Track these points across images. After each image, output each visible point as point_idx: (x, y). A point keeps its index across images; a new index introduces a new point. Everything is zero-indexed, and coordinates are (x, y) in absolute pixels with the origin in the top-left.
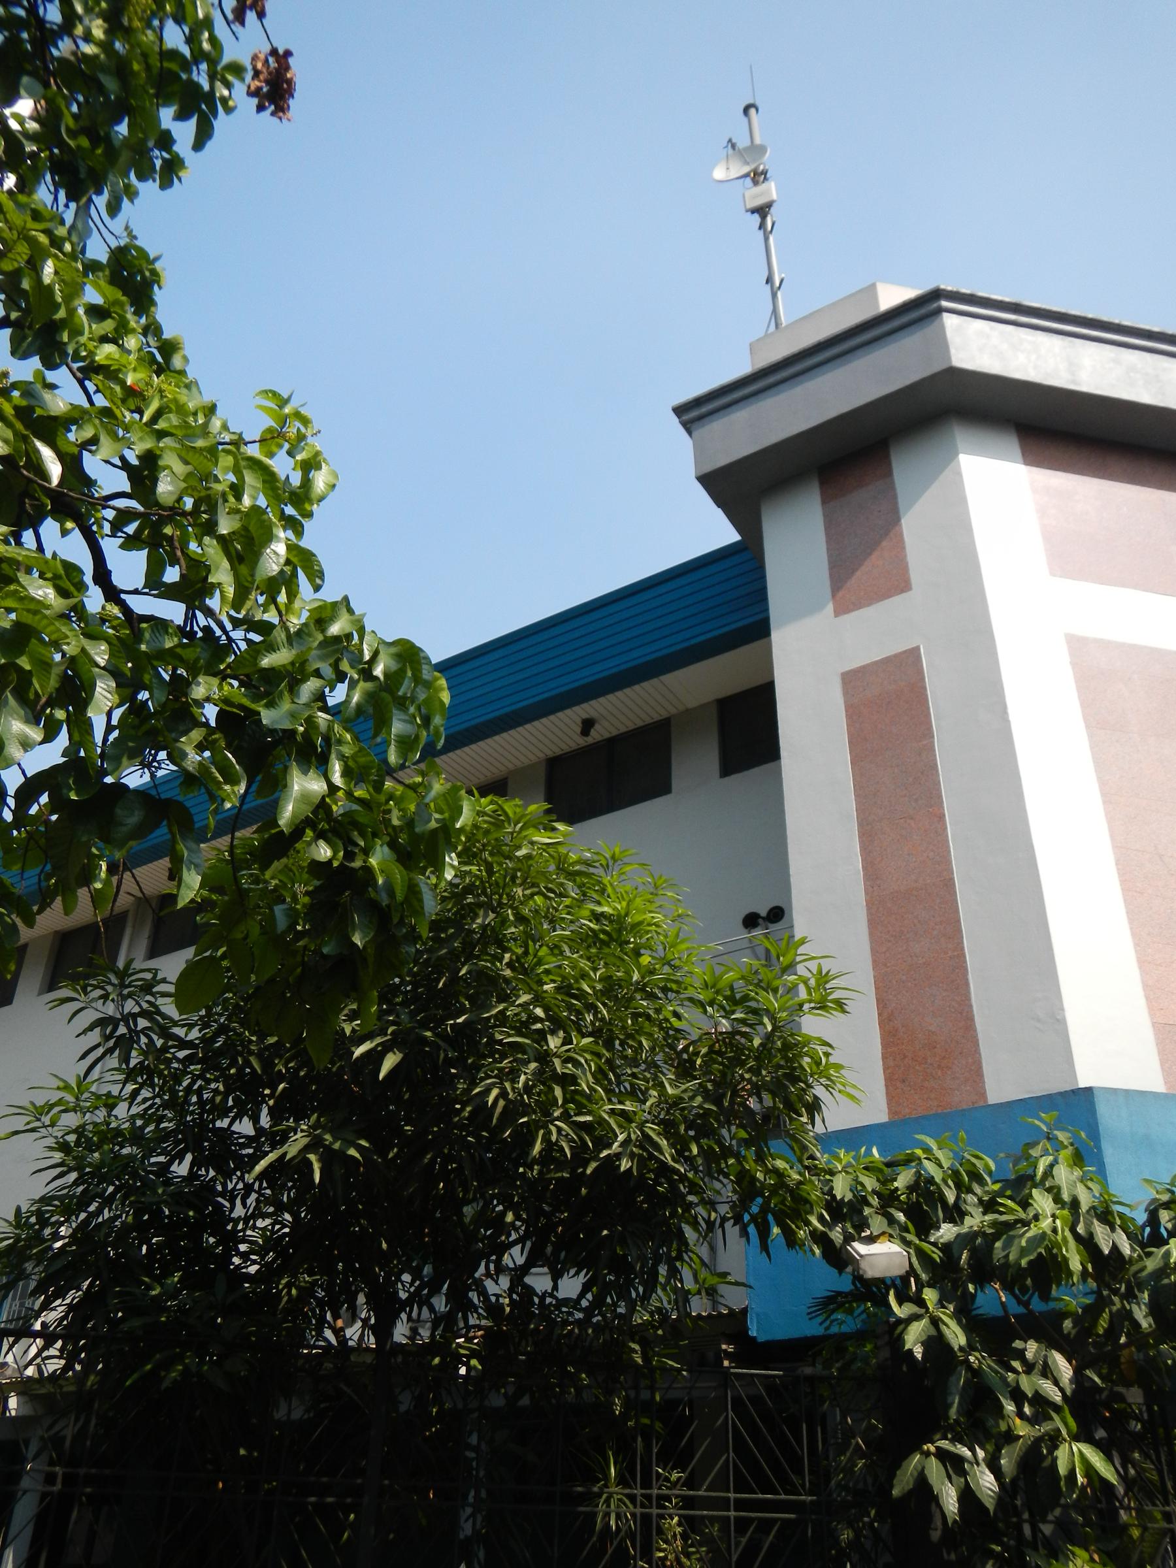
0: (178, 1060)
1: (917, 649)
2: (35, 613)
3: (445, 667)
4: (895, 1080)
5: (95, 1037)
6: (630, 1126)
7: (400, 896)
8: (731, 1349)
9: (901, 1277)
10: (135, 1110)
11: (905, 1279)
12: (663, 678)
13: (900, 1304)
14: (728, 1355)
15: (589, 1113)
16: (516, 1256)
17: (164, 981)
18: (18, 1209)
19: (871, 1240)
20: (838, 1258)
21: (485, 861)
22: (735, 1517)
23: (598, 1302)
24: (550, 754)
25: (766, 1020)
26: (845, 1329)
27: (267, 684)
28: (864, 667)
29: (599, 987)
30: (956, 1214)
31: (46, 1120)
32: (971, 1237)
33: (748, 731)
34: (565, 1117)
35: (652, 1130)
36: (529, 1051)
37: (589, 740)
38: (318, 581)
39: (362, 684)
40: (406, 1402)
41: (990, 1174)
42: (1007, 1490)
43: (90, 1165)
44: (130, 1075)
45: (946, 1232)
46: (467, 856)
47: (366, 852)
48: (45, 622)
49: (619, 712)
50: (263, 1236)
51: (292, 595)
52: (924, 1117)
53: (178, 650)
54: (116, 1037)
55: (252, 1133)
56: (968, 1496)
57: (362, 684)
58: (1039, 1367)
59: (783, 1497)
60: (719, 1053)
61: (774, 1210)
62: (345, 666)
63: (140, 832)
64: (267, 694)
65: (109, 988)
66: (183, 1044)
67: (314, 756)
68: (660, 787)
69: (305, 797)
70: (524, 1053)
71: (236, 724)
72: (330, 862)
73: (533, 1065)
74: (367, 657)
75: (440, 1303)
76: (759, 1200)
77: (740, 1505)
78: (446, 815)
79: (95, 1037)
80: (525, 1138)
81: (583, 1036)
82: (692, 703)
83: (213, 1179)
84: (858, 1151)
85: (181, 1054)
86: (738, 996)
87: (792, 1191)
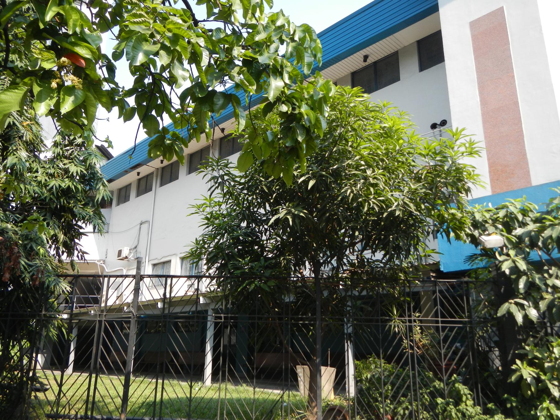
0: (239, 189)
1: (503, 7)
2: (179, 28)
3: (320, 35)
4: (493, 180)
5: (212, 183)
6: (398, 199)
7: (313, 122)
8: (434, 275)
9: (500, 247)
10: (228, 206)
11: (502, 248)
12: (394, 35)
13: (500, 255)
14: (433, 277)
15: (383, 196)
16: (358, 246)
17: (231, 163)
18: (196, 239)
19: (489, 235)
20: (475, 241)
21: (339, 109)
22: (442, 326)
23: (389, 260)
24: (352, 71)
25: (449, 160)
26: (478, 266)
27: (259, 47)
28: (479, 18)
29: (384, 152)
30: (523, 224)
31: (201, 210)
32: (529, 233)
33: (431, 52)
34: (374, 198)
35: (407, 201)
36: (360, 176)
37: (367, 63)
38: (271, 4)
39: (291, 44)
40: (326, 293)
41: (536, 210)
42: (542, 316)
43: (216, 224)
44: (225, 195)
45: (519, 231)
46: (333, 108)
47: (299, 107)
48: (183, 31)
49: (378, 51)
50: (272, 245)
51: (262, 12)
52: (506, 192)
53: (226, 38)
54: (219, 182)
55: (264, 213)
56: (526, 317)
57: (291, 44)
58: (555, 276)
59: (458, 319)
60: (430, 173)
61: (450, 227)
62: (284, 37)
63: (223, 107)
64: (259, 51)
65: (214, 167)
66: (240, 184)
67: (278, 72)
68: (396, 78)
69: (277, 88)
70: (358, 177)
71: (248, 63)
72: (287, 112)
73: (362, 181)
74: (292, 33)
75: (334, 262)
76: (446, 224)
77: (443, 322)
78: (325, 92)
79: (212, 183)
80: (361, 205)
81: (379, 169)
82: (406, 44)
83: (255, 227)
84: (483, 204)
85: (240, 187)
86: (437, 152)
87: (458, 221)
